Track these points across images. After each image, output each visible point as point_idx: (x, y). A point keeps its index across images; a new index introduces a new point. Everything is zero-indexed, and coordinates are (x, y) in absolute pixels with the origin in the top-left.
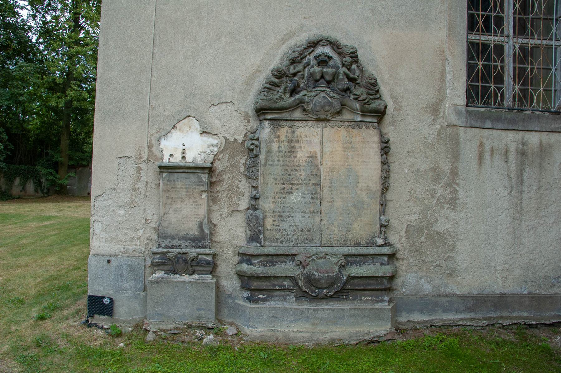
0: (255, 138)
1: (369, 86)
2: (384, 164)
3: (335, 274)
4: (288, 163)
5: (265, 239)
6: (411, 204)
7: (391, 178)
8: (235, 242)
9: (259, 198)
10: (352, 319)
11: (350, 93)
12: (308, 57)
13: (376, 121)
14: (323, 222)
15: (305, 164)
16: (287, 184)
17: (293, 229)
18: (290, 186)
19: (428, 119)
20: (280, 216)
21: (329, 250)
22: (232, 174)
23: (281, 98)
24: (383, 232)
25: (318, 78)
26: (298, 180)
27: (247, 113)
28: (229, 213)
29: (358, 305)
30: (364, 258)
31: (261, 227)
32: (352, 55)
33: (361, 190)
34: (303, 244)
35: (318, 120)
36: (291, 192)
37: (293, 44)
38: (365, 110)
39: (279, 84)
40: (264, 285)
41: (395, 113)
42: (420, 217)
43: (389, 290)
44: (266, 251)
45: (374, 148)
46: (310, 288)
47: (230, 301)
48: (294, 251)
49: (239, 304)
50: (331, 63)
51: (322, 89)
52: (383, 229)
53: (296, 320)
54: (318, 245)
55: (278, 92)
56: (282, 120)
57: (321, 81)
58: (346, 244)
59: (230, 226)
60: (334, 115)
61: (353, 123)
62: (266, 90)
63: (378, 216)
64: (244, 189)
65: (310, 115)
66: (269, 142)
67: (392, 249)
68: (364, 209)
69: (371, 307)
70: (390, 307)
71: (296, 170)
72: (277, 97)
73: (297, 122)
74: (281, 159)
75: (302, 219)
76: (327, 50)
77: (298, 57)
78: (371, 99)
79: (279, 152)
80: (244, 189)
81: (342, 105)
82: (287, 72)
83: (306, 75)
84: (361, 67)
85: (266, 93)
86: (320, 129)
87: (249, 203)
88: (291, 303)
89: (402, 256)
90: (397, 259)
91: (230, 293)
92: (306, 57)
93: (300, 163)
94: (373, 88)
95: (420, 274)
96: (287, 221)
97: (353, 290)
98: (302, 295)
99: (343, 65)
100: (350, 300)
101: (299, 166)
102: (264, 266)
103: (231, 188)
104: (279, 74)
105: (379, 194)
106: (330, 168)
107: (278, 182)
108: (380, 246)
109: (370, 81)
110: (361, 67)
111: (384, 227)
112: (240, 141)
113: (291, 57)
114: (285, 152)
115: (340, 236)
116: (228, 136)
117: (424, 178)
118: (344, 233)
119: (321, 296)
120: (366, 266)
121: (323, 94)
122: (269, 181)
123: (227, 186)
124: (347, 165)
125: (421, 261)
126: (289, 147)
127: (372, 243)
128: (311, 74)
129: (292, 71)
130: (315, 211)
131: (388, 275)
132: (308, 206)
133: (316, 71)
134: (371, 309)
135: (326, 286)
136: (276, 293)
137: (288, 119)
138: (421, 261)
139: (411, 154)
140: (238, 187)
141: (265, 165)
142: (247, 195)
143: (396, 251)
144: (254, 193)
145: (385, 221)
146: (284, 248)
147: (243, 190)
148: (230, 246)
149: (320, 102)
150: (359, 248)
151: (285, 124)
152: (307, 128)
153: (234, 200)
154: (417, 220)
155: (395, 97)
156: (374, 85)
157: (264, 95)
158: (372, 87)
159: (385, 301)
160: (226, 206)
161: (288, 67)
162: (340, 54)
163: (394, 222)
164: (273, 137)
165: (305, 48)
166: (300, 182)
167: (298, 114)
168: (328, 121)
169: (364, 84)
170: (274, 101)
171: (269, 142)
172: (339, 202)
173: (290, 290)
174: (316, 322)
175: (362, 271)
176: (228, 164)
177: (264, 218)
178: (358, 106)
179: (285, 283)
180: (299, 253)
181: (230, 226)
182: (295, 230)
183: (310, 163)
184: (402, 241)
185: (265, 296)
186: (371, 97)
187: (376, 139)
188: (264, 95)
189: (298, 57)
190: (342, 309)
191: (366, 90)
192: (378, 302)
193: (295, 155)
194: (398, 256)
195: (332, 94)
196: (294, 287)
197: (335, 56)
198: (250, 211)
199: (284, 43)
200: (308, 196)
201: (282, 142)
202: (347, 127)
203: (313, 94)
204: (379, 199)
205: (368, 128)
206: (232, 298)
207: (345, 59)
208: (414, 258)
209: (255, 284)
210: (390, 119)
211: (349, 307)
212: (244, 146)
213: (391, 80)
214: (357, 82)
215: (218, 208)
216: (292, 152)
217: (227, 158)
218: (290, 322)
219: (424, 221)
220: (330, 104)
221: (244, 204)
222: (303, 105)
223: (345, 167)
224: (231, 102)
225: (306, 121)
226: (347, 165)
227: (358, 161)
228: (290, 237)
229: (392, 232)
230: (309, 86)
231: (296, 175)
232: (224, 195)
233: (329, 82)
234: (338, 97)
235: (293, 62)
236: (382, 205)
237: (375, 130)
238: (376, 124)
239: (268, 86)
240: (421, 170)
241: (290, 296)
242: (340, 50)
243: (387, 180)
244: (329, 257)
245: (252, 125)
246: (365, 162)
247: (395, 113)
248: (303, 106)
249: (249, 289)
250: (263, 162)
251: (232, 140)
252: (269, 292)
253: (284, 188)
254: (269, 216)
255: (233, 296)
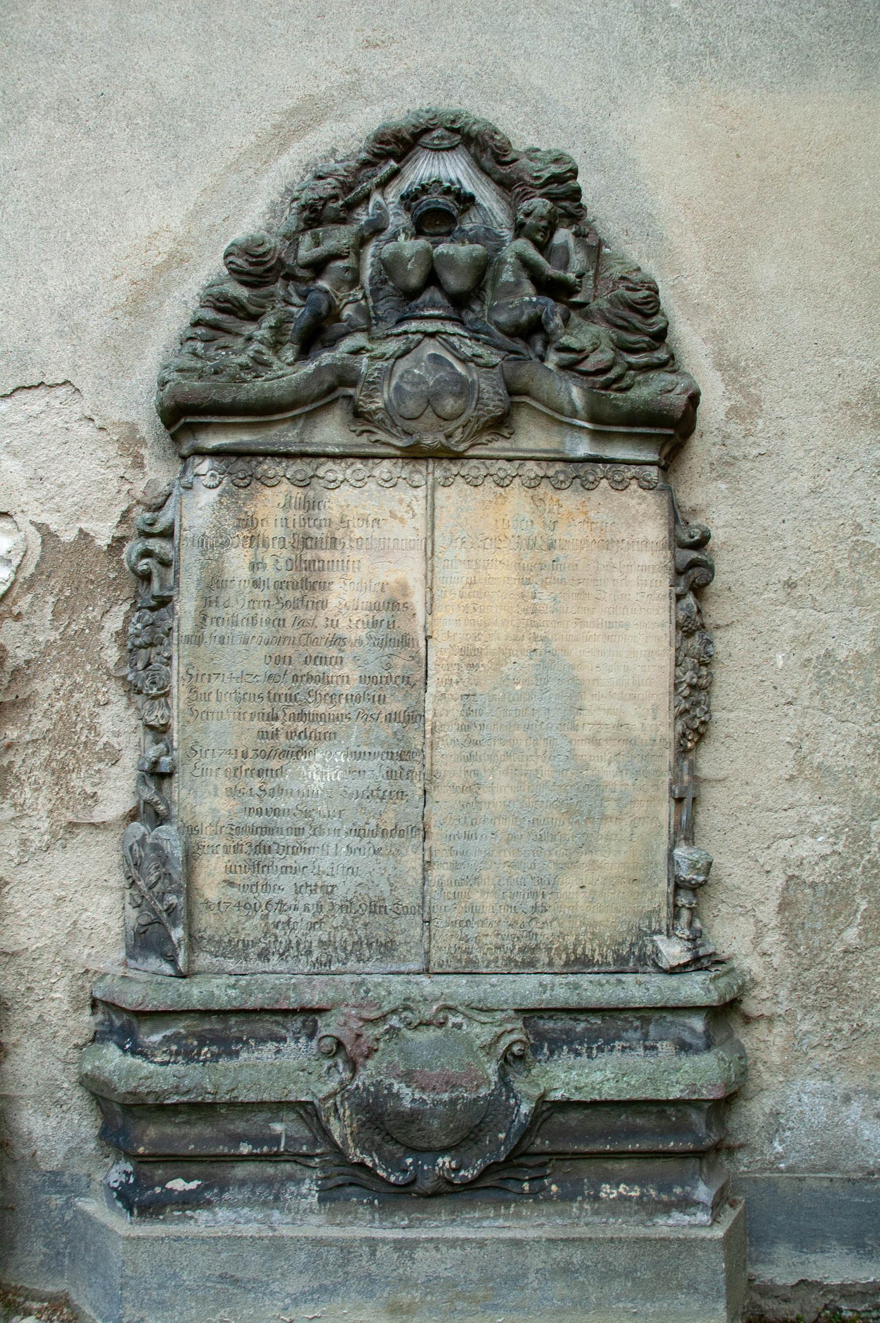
0: (158, 528)
1: (627, 313)
2: (689, 634)
3: (483, 1092)
4: (290, 631)
5: (193, 942)
6: (803, 794)
7: (716, 690)
8: (81, 953)
9: (170, 775)
10: (560, 1284)
11: (546, 344)
12: (376, 197)
13: (652, 457)
14: (435, 874)
15: (362, 633)
16: (289, 717)
17: (312, 900)
18: (300, 726)
19: (868, 452)
20: (258, 847)
21: (461, 988)
22: (69, 675)
23: (259, 364)
24: (685, 914)
25: (414, 280)
26: (333, 698)
27: (133, 428)
28: (54, 835)
29: (579, 1222)
30: (608, 1024)
31: (177, 892)
32: (554, 188)
33: (594, 741)
34: (352, 964)
35: (414, 454)
36: (301, 751)
37: (323, 150)
38: (607, 410)
39: (253, 309)
40: (189, 1136)
41: (735, 429)
42: (840, 848)
43: (712, 1153)
44: (195, 993)
45: (645, 569)
46: (379, 1150)
47: (57, 1200)
48: (313, 997)
49: (88, 1218)
50: (470, 223)
51: (431, 327)
52: (683, 900)
53: (323, 1289)
54: (415, 966)
55: (250, 339)
56: (266, 454)
57: (426, 296)
58: (532, 964)
59: (61, 885)
60: (479, 432)
61: (559, 466)
62: (201, 331)
63: (664, 847)
64: (117, 735)
65: (382, 436)
66: (214, 545)
67: (722, 983)
68: (604, 817)
69: (642, 1231)
70: (719, 1233)
71: (322, 660)
72: (243, 359)
73: (330, 464)
74: (264, 614)
75: (347, 860)
76: (454, 169)
77: (335, 197)
78: (631, 366)
79: (256, 584)
80: (117, 735)
81: (512, 393)
82: (290, 261)
83: (367, 272)
84: (591, 241)
85: (199, 345)
86: (421, 493)
87: (136, 793)
88: (305, 1219)
89: (766, 1009)
90: (748, 1020)
91: (54, 1164)
92: (367, 197)
93: (343, 630)
94: (641, 321)
95: (843, 1083)
96: (286, 869)
97: (562, 1156)
98: (347, 1183)
99: (519, 229)
100: (549, 1199)
101: (338, 641)
102: (190, 1056)
103: (63, 734)
104: (256, 267)
105: (669, 755)
106: (465, 652)
107: (251, 707)
108: (672, 971)
109: (628, 294)
110: (591, 241)
111: (691, 892)
112: (103, 542)
113: (307, 196)
114: (280, 585)
115: (505, 930)
116: (53, 522)
117: (851, 687)
118: (523, 918)
119: (427, 1184)
120: (617, 1054)
121: (431, 348)
122: (213, 705)
123: (47, 724)
124: (535, 638)
125: (846, 1026)
126: (295, 564)
127: (642, 959)
128: (388, 267)
129: (306, 251)
130: (403, 825)
131: (705, 1094)
132: (373, 805)
133: (407, 253)
134: (637, 1240)
135: (446, 1142)
136: (241, 1171)
137: (293, 449)
138: (846, 1026)
139: (800, 591)
140: (92, 728)
141: (197, 640)
142: (130, 761)
143: (742, 988)
144: (152, 752)
145: (693, 866)
146: (277, 981)
147: (114, 741)
148: (58, 969)
149: (421, 380)
150: (584, 980)
151: (280, 471)
152: (372, 486)
153: (75, 781)
154: (824, 858)
155: (734, 365)
156: (647, 309)
157: (194, 354)
158: (636, 319)
159: (697, 1203)
160: (43, 803)
161: (292, 239)
162: (505, 185)
163: (731, 869)
164: (229, 523)
165: (365, 164)
166: (342, 707)
167: (331, 431)
168: (457, 457)
169: (606, 305)
170: (233, 378)
171: (214, 545)
172: (500, 790)
173: (297, 1158)
174: (404, 1297)
175: (598, 1076)
176: (54, 636)
177: (190, 857)
178: (576, 394)
179: (278, 1127)
180: (335, 1004)
181: (61, 885)
182: (320, 907)
183: (382, 631)
184: (765, 946)
185: (193, 1185)
186: (632, 359)
187: (654, 531)
188: (194, 354)
189: (335, 197)
190: (517, 1243)
191: (614, 334)
192: (667, 1208)
193: (318, 596)
194: (751, 1006)
195: (469, 348)
196: (314, 1144)
197: (487, 196)
198: (138, 828)
199: (283, 147)
200: (373, 764)
201: (265, 545)
202: (533, 484)
203: (392, 346)
204: (667, 778)
205: (620, 486)
206: (63, 1189)
207: (525, 206)
208: (817, 1016)
209: (152, 1132)
210: (716, 452)
211: (547, 1232)
212: (120, 562)
213: (716, 297)
214: (578, 299)
215: (11, 813)
216: (306, 584)
217: (49, 609)
218: (296, 1301)
219: (856, 864)
220: (464, 389)
221: (118, 793)
222: (351, 391)
223: (526, 644)
224: (66, 382)
225: (365, 457)
226: (535, 638)
227: (579, 622)
228: (299, 933)
229: (724, 908)
230: (378, 319)
231: (324, 679)
232: (37, 761)
233: (460, 302)
234: (496, 360)
235: (314, 216)
236: (679, 801)
237: (649, 496)
238: (653, 472)
239: (210, 315)
240: (842, 654)
241: (299, 1182)
242: (504, 170)
243: (702, 696)
244: (459, 1019)
245: (151, 475)
246: (610, 625)
247: (735, 429)
248: (350, 397)
249: (130, 1156)
250: (187, 627)
251: (69, 536)
252: (213, 1171)
253: (275, 734)
254: (214, 850)
255: (66, 1179)
